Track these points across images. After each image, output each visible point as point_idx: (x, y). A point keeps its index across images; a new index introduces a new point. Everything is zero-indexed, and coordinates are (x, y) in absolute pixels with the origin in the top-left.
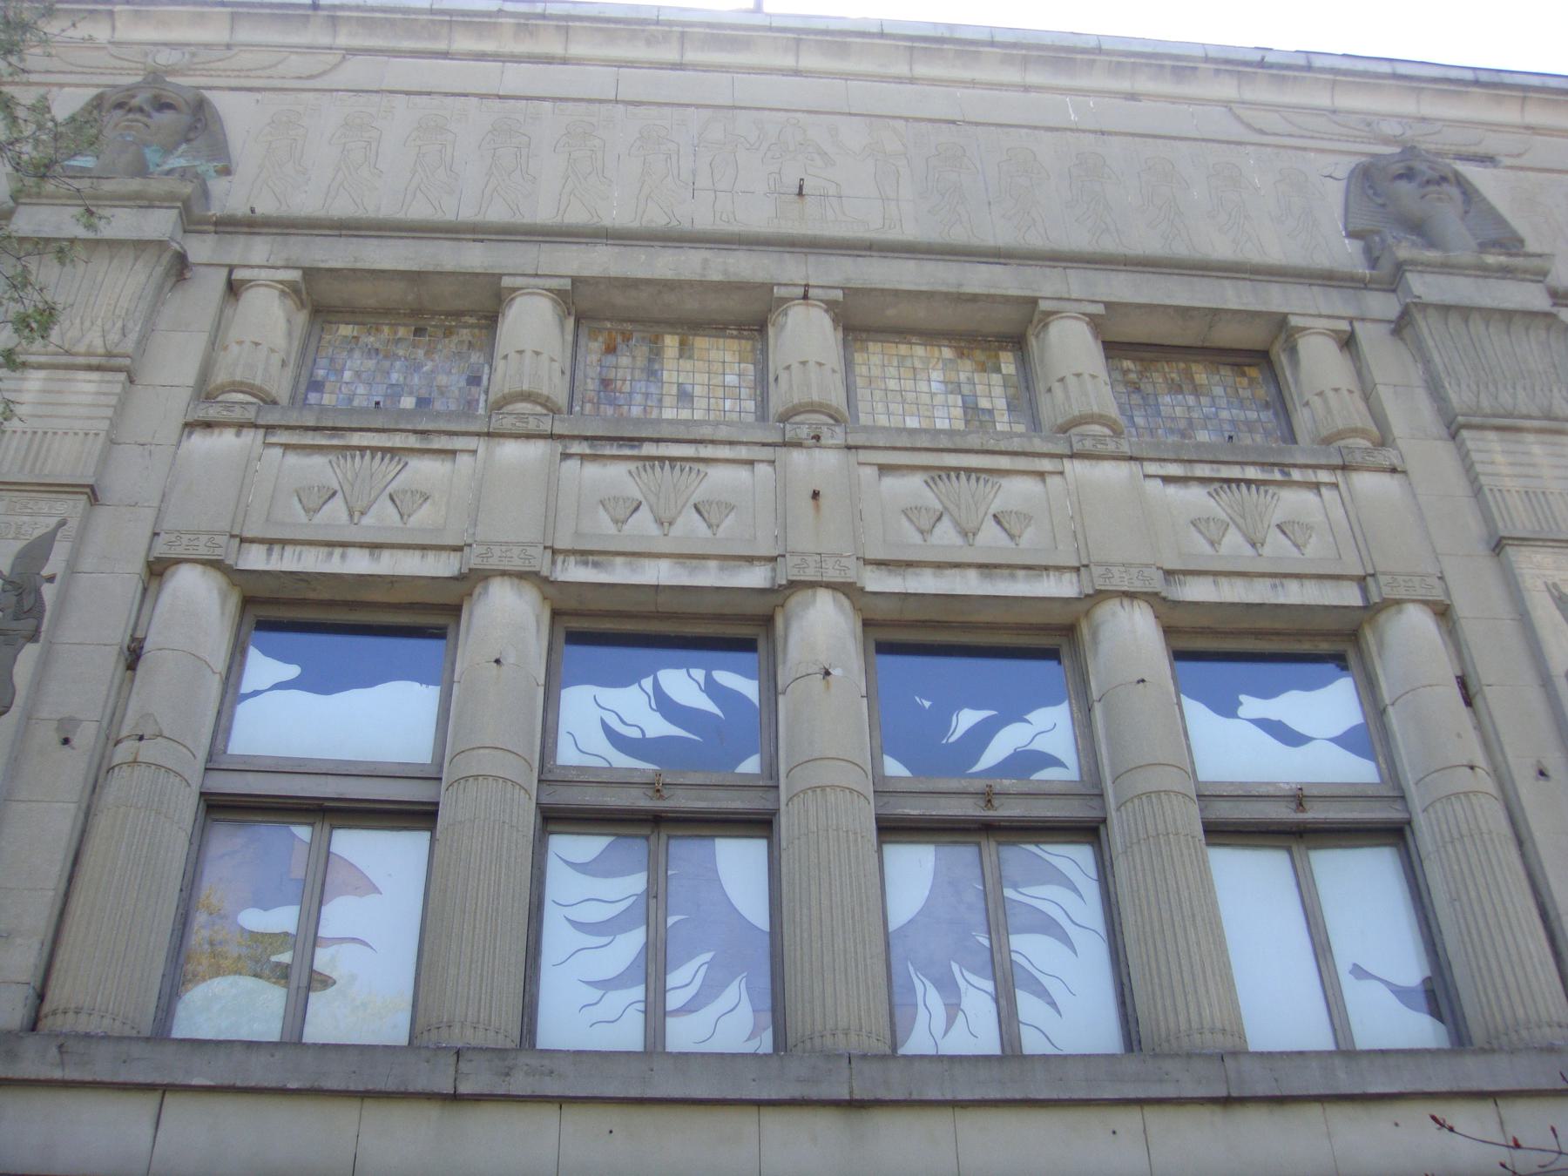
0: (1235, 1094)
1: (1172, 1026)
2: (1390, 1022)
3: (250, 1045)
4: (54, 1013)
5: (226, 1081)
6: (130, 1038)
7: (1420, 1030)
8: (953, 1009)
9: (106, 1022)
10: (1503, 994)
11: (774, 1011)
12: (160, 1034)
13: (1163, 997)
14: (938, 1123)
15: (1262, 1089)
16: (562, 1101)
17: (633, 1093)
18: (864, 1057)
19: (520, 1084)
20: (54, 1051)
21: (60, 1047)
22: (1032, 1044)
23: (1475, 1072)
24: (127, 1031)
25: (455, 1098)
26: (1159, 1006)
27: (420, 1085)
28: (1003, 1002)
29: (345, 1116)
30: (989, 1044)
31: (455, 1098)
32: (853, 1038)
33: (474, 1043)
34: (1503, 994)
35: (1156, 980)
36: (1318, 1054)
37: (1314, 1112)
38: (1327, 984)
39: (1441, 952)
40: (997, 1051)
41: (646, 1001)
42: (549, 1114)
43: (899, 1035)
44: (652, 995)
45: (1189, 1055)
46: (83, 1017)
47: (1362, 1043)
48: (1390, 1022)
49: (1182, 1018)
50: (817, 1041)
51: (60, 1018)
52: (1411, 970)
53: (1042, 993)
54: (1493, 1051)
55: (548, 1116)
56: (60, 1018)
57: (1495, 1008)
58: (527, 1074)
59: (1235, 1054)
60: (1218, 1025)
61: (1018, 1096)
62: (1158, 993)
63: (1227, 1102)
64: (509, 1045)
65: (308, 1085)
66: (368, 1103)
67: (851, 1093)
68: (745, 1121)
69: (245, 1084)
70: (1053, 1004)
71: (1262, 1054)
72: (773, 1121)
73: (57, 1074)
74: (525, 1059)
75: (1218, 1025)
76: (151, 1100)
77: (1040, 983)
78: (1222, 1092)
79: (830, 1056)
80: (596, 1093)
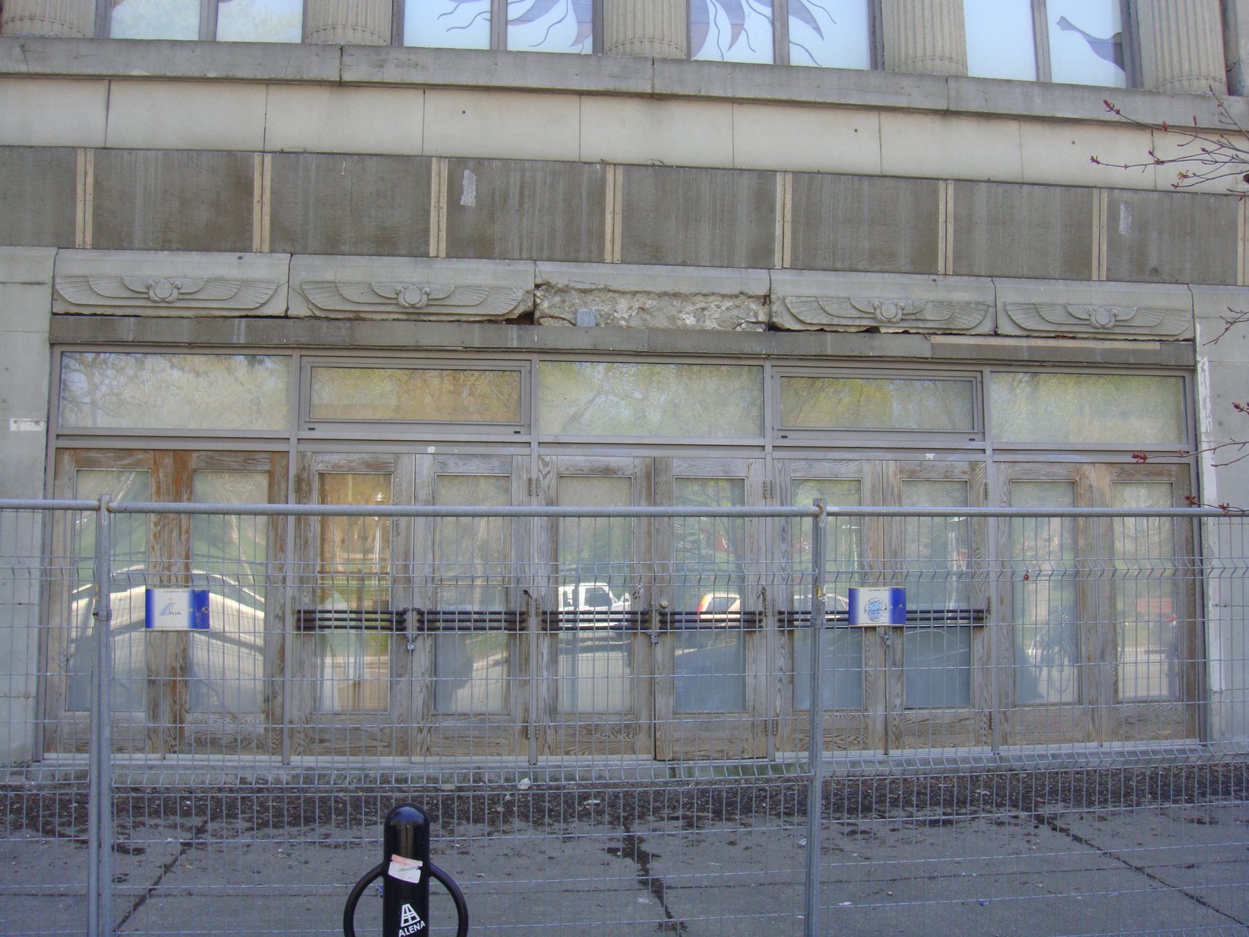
0: (953, 108)
1: (911, 52)
2: (1082, 64)
3: (175, 43)
4: (13, 20)
5: (159, 72)
6: (78, 39)
7: (1106, 73)
8: (738, 28)
9: (57, 27)
10: (1175, 51)
11: (594, 23)
12: (102, 34)
13: (906, 30)
14: (721, 114)
15: (973, 107)
16: (425, 87)
17: (482, 82)
18: (664, 60)
19: (391, 74)
20: (17, 50)
21: (22, 46)
22: (798, 58)
23: (1140, 109)
24: (74, 34)
25: (341, 84)
26: (902, 36)
27: (312, 74)
28: (778, 25)
29: (255, 98)
30: (764, 55)
31: (341, 84)
32: (657, 45)
33: (354, 42)
34: (1175, 51)
35: (902, 15)
36: (1022, 83)
37: (1013, 127)
38: (1038, 31)
39: (1133, 14)
40: (769, 61)
41: (491, 12)
42: (415, 98)
43: (693, 46)
44: (496, 7)
45: (921, 76)
46: (37, 24)
47: (1057, 79)
48: (1082, 64)
49: (919, 46)
50: (628, 46)
51: (18, 24)
52: (1106, 25)
53: (810, 20)
54: (1158, 93)
55: (414, 100)
56: (18, 23)
57: (1167, 61)
58: (397, 66)
59: (957, 78)
60: (947, 55)
61: (784, 98)
62: (902, 26)
63: (946, 114)
64: (382, 43)
65: (223, 74)
66: (272, 89)
67: (653, 87)
68: (569, 107)
69: (174, 74)
70: (818, 29)
71: (978, 79)
72: (591, 107)
73: (23, 68)
74: (394, 54)
75: (947, 55)
76: (101, 88)
77: (809, 12)
78: (942, 106)
79: (640, 58)
80: (453, 82)
